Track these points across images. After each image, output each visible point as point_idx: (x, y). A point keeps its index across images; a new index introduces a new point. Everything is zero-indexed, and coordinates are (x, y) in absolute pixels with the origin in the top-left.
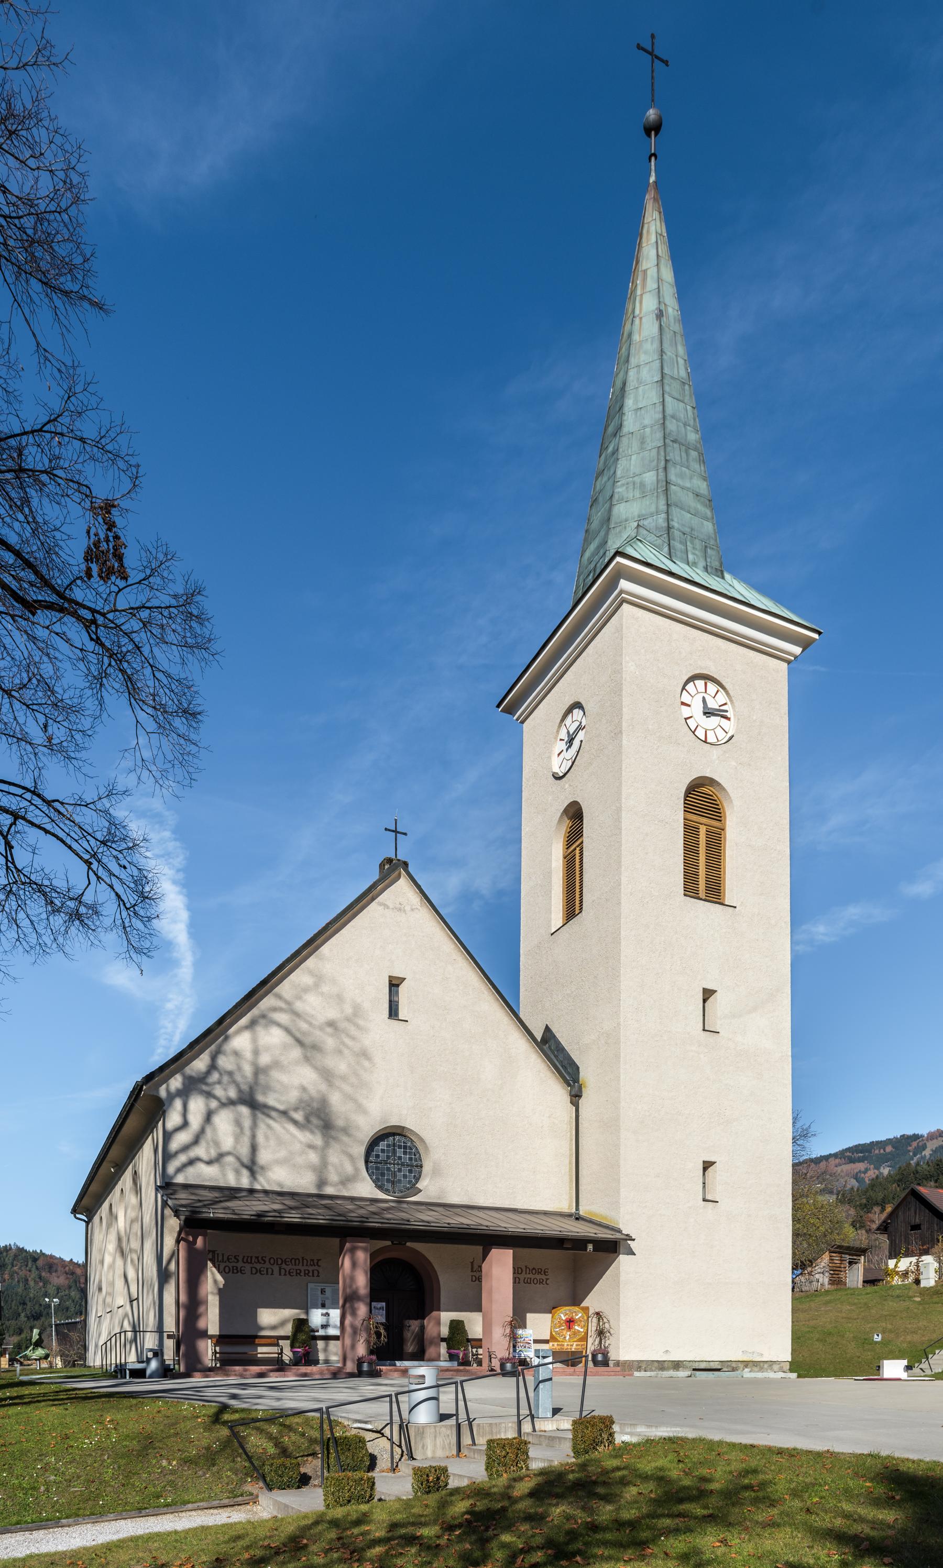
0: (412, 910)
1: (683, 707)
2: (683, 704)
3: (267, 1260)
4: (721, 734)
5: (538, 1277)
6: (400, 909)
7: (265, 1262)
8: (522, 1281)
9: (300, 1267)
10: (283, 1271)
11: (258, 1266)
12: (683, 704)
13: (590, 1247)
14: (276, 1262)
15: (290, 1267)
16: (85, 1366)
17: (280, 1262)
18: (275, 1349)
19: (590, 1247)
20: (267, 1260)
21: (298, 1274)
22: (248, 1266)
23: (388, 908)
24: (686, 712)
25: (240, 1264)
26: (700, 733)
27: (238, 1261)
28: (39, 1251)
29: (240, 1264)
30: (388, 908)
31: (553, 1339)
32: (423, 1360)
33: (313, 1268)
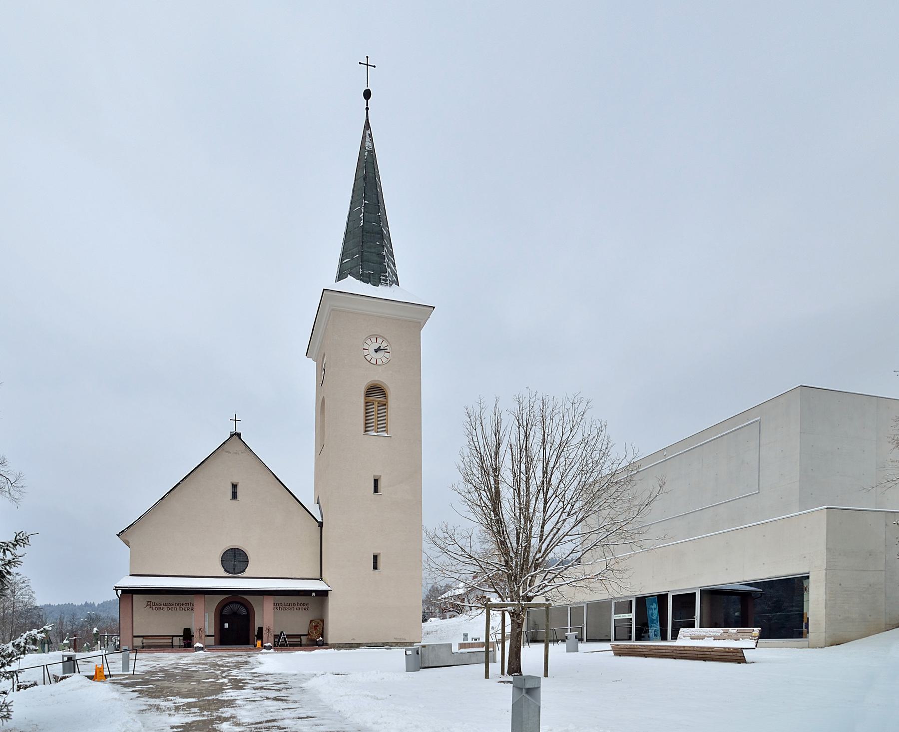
0: (242, 453)
1: (364, 350)
2: (364, 349)
3: (162, 604)
4: (384, 360)
5: (303, 607)
6: (236, 453)
7: (173, 605)
8: (295, 609)
9: (189, 607)
10: (181, 609)
11: (170, 607)
12: (364, 349)
13: (314, 594)
14: (178, 605)
15: (185, 607)
16: (327, 644)
17: (180, 605)
18: (299, 640)
19: (314, 594)
20: (162, 604)
21: (289, 609)
22: (166, 607)
23: (230, 453)
24: (366, 352)
25: (162, 607)
26: (373, 361)
27: (161, 605)
28: (92, 603)
29: (162, 607)
30: (230, 453)
31: (309, 634)
32: (249, 645)
33: (292, 607)
